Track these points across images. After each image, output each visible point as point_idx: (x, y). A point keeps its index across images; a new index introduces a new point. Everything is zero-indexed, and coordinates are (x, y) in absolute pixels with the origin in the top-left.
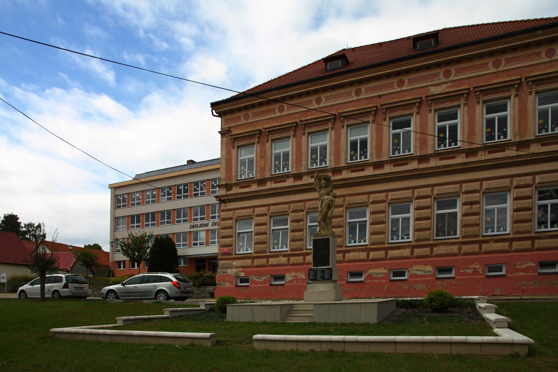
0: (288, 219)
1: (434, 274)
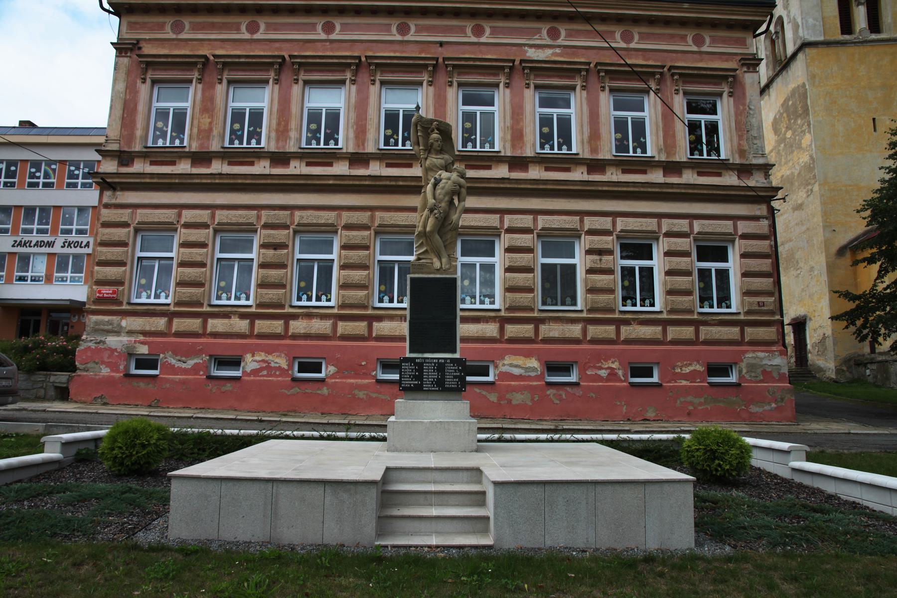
0: (253, 240)
1: (542, 373)
